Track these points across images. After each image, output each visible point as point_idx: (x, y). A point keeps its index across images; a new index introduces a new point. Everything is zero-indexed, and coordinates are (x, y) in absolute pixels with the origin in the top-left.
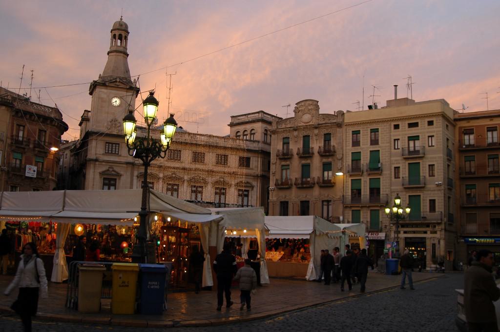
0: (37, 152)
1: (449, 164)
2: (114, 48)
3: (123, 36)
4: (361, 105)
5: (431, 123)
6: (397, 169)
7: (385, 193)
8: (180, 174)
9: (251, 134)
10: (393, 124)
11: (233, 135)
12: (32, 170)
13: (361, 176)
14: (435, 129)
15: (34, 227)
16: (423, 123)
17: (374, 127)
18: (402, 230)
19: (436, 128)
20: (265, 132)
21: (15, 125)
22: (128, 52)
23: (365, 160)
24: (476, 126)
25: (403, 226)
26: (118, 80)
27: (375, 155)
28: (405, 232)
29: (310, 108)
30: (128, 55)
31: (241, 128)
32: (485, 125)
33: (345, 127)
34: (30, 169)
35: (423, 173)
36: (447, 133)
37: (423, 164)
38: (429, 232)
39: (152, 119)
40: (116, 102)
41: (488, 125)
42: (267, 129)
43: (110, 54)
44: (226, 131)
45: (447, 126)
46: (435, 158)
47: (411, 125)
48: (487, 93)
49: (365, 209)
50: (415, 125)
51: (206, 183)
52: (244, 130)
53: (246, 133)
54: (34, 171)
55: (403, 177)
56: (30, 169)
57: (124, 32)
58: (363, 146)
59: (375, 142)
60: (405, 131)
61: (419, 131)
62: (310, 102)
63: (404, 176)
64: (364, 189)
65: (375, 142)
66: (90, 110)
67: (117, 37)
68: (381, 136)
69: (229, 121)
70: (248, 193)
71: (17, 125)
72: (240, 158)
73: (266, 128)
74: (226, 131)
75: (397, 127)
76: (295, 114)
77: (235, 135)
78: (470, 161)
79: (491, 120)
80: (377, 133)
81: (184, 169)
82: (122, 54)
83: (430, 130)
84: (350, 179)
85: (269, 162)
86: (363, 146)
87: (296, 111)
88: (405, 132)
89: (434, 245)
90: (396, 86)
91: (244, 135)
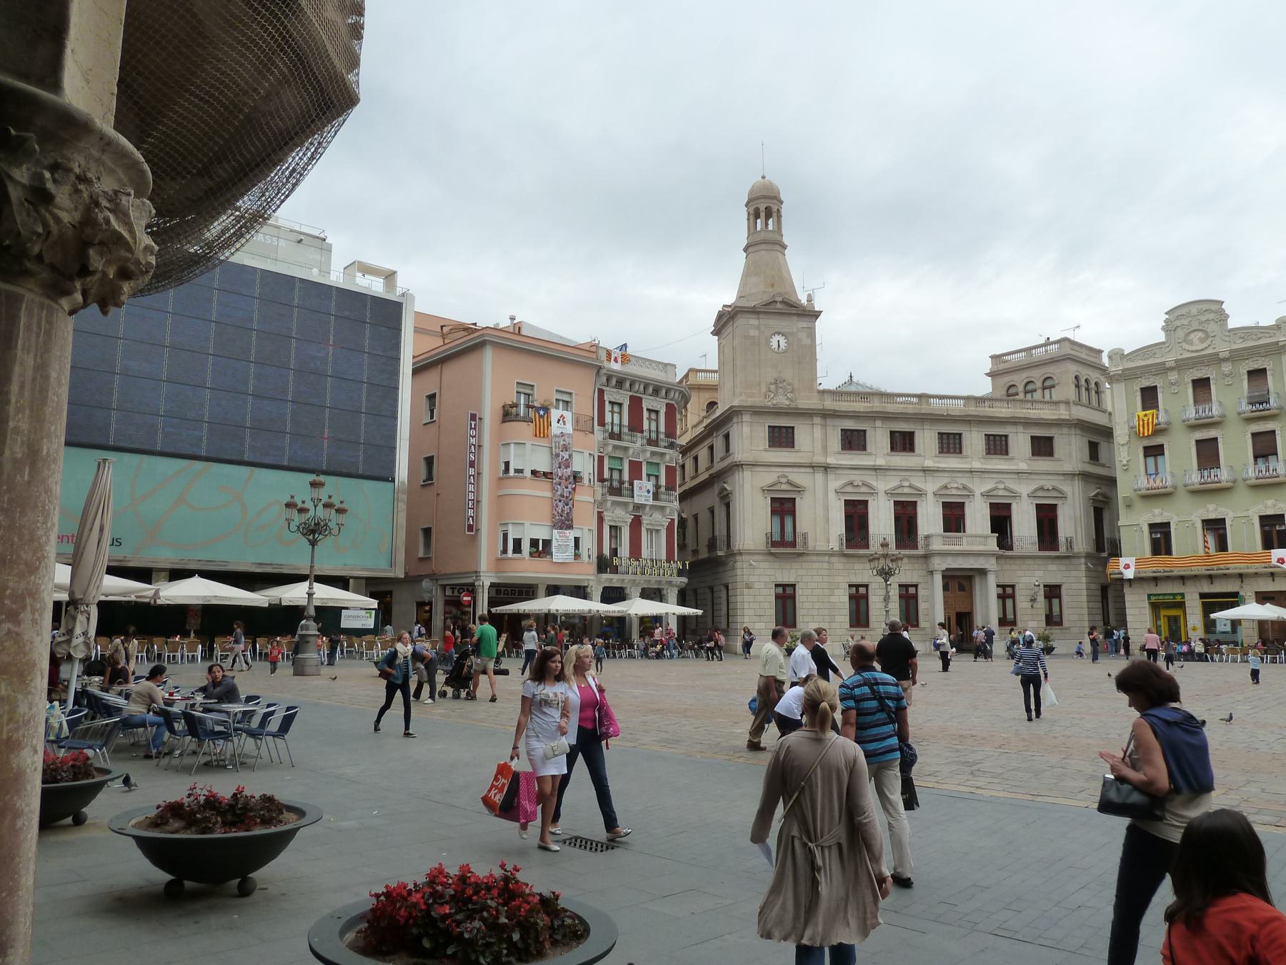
0: (648, 454)
2: (759, 238)
8: (918, 482)
9: (1044, 388)
10: (1244, 368)
11: (1002, 392)
12: (644, 489)
22: (786, 240)
26: (779, 299)
29: (1203, 318)
30: (784, 247)
31: (1008, 380)
33: (71, 320)
40: (778, 341)
43: (750, 250)
44: (984, 387)
48: (157, 766)
52: (1026, 381)
53: (1030, 387)
54: (648, 492)
56: (640, 488)
62: (1204, 307)
66: (717, 369)
67: (763, 215)
69: (988, 365)
72: (1033, 438)
73: (1078, 373)
74: (984, 387)
76: (1167, 336)
77: (1005, 393)
81: (925, 471)
82: (763, 246)
85: (1282, 371)
87: (1169, 328)
91: (1044, 388)
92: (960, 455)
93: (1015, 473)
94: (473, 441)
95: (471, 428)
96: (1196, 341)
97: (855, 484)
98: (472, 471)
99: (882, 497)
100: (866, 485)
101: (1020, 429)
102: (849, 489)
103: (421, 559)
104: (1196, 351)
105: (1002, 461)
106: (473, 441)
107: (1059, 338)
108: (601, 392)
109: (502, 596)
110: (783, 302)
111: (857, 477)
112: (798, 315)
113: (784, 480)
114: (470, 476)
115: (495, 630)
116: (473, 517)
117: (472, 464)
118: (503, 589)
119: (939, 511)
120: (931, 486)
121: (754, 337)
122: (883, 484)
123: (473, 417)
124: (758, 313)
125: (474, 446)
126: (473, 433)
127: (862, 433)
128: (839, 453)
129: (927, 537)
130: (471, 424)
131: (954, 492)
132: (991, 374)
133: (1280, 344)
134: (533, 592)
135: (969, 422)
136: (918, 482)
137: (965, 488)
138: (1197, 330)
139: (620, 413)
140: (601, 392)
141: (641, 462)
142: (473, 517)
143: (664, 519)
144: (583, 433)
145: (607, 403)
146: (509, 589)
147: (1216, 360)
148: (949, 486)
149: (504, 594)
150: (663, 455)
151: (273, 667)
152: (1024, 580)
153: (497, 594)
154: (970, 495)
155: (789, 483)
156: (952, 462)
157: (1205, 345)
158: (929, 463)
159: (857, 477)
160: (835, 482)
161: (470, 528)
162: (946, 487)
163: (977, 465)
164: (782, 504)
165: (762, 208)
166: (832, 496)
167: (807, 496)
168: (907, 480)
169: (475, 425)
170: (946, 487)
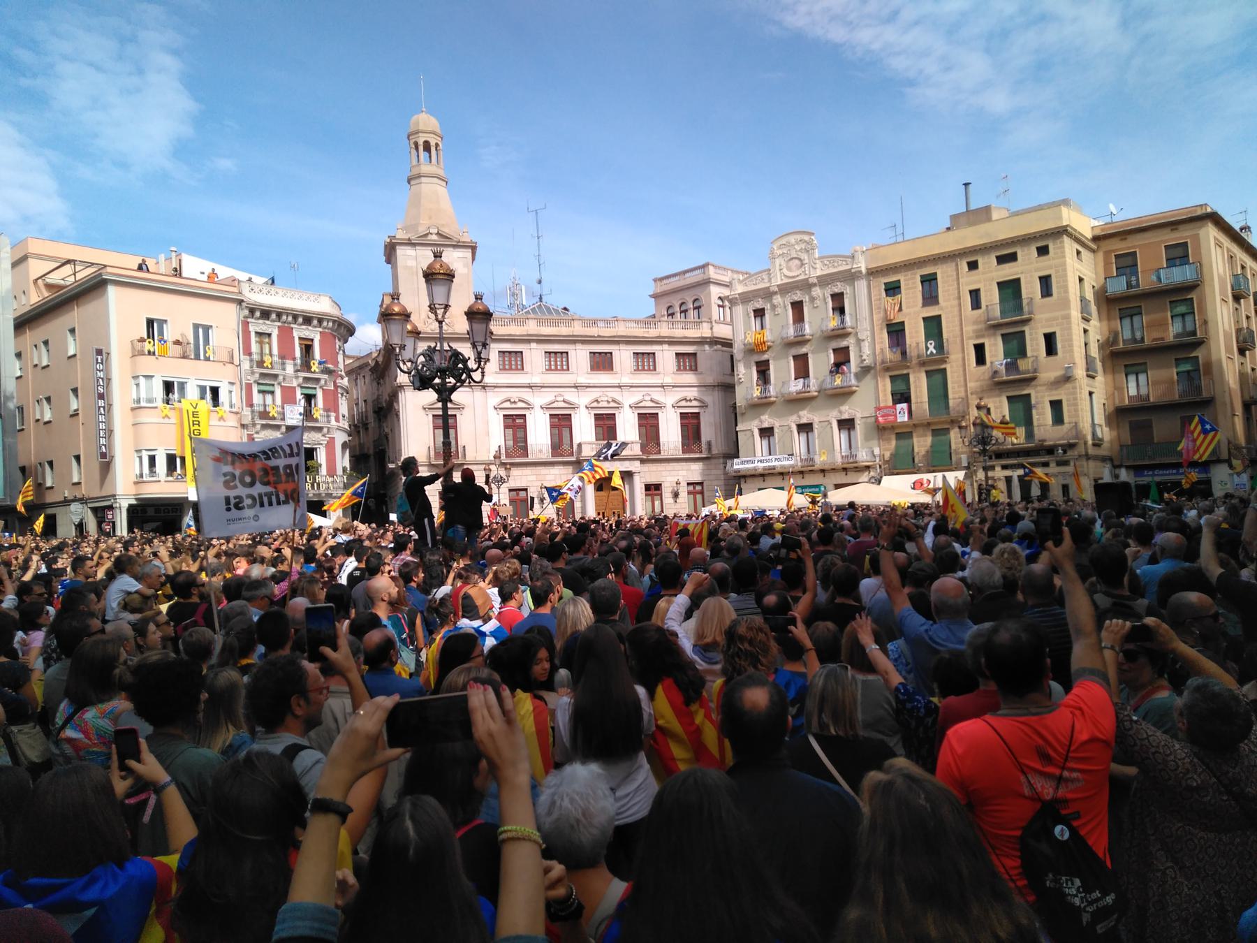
1: (1087, 328)
3: (433, 143)
4: (899, 231)
5: (973, 266)
6: (980, 349)
7: (957, 396)
13: (908, 367)
14: (1052, 262)
15: (965, 544)
16: (1027, 255)
17: (928, 270)
18: (998, 463)
19: (1054, 259)
20: (720, 303)
21: (253, 335)
23: (915, 336)
24: (1139, 246)
25: (999, 455)
27: (933, 326)
28: (1004, 467)
32: (1114, 251)
34: (292, 411)
35: (1033, 350)
36: (1079, 267)
37: (1031, 334)
38: (1053, 465)
39: (443, 306)
41: (1116, 250)
42: (722, 295)
45: (1078, 253)
46: (1055, 319)
47: (1002, 260)
49: (920, 431)
50: (1012, 257)
51: (529, 407)
55: (992, 363)
57: (432, 135)
58: (908, 311)
59: (930, 297)
60: (991, 272)
61: (994, 274)
63: (994, 359)
64: (916, 392)
65: (930, 297)
68: (944, 288)
69: (652, 288)
70: (525, 421)
71: (256, 333)
75: (1043, 251)
78: (1131, 316)
79: (1122, 240)
80: (933, 282)
82: (436, 180)
83: (1040, 265)
84: (923, 369)
86: (908, 311)
88: (990, 275)
89: (1065, 488)
90: (966, 185)
92: (567, 372)
93: (527, 387)
94: (101, 374)
95: (97, 363)
96: (794, 268)
97: (512, 400)
98: (101, 403)
99: (627, 409)
100: (523, 401)
101: (666, 347)
102: (507, 405)
103: (74, 484)
104: (793, 277)
105: (649, 376)
106: (101, 374)
107: (427, 298)
108: (246, 324)
109: (162, 514)
110: (438, 234)
111: (514, 394)
112: (454, 246)
113: (648, 398)
114: (99, 408)
115: (953, 697)
116: (105, 446)
117: (101, 396)
118: (162, 508)
119: (591, 422)
120: (582, 399)
121: (412, 267)
122: (539, 399)
123: (99, 352)
124: (414, 245)
125: (102, 379)
126: (100, 367)
127: (565, 355)
128: (496, 373)
129: (580, 445)
130: (97, 359)
131: (605, 404)
132: (656, 296)
133: (853, 271)
134: (181, 509)
135: (618, 343)
136: (571, 396)
137: (614, 401)
138: (796, 258)
139: (270, 344)
140: (246, 324)
141: (295, 388)
142: (105, 446)
143: (324, 438)
144: (222, 364)
145: (253, 335)
146: (170, 508)
147: (806, 286)
148: (599, 400)
149: (164, 512)
150: (318, 380)
151: (587, 836)
152: (669, 479)
153: (156, 513)
154: (619, 406)
155: (652, 401)
156: (603, 378)
157: (800, 271)
158: (582, 380)
159: (514, 394)
160: (494, 398)
161: (103, 455)
162: (597, 401)
163: (626, 380)
164: (514, 420)
165: (421, 143)
166: (492, 411)
167: (465, 412)
168: (561, 395)
169: (102, 360)
170: (597, 401)
